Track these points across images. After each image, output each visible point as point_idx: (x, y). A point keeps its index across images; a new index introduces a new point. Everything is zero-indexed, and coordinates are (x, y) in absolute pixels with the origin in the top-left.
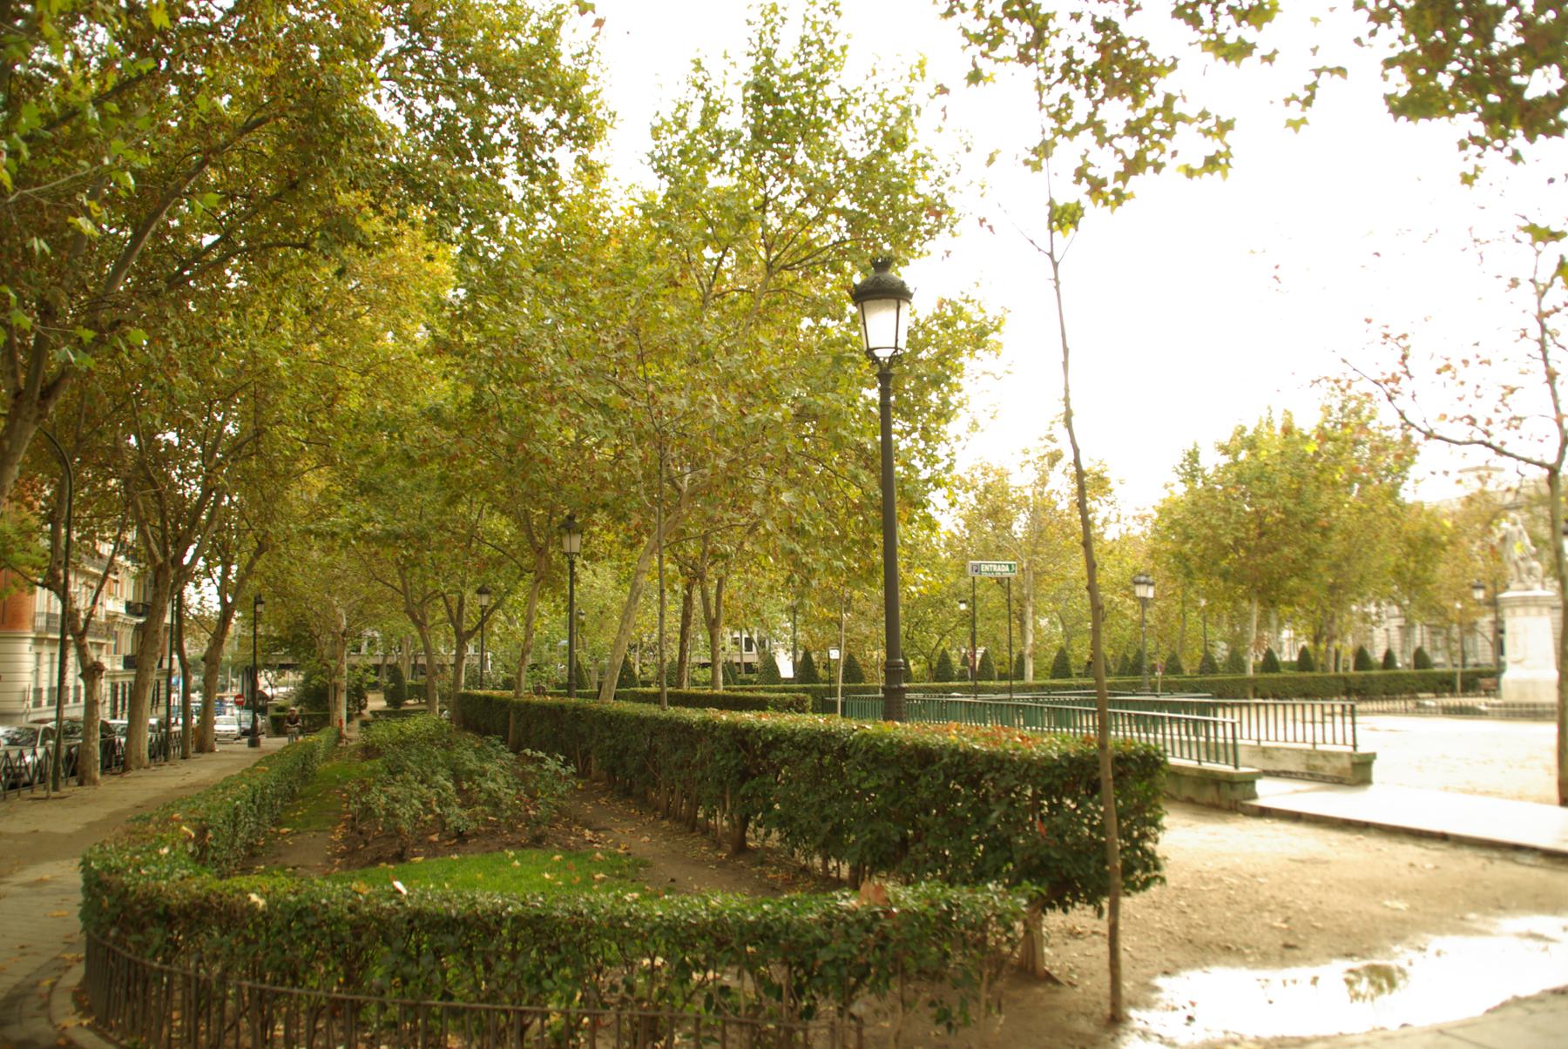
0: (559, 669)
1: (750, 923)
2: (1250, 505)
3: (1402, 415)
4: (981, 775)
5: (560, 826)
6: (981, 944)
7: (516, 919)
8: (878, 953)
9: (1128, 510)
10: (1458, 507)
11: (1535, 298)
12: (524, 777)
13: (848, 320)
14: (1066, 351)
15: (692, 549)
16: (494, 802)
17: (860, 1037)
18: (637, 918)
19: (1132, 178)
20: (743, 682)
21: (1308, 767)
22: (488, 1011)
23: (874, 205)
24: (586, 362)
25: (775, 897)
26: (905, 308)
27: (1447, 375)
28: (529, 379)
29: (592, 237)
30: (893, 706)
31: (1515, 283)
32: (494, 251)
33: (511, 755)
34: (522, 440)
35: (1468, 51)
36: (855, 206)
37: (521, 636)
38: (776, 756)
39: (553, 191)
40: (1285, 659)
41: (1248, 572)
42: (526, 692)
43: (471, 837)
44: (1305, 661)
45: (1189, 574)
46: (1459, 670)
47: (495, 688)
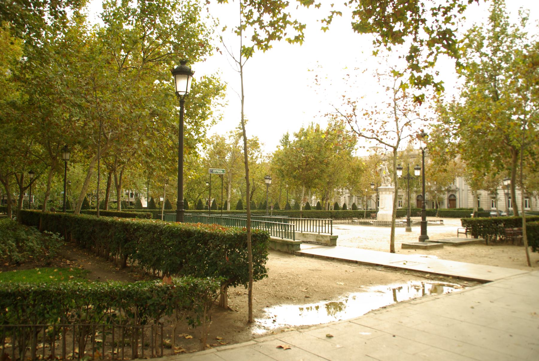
0: (60, 202)
1: (123, 291)
2: (304, 154)
3: (352, 128)
4: (208, 240)
5: (57, 259)
6: (205, 298)
7: (35, 292)
8: (168, 301)
9: (264, 154)
10: (368, 159)
11: (394, 94)
12: (44, 241)
13: (171, 81)
14: (243, 97)
15: (111, 160)
16: (32, 251)
17: (162, 330)
18: (82, 290)
19: (271, 41)
20: (129, 208)
21: (317, 240)
22: (23, 327)
23: (183, 41)
24: (74, 89)
25: (133, 282)
26: (191, 79)
27: (366, 116)
28: (52, 94)
29: (79, 43)
30: (179, 217)
31: (388, 89)
32: (39, 44)
33: (40, 233)
34: (47, 117)
35: (379, 13)
36: (176, 41)
37: (45, 190)
38: (138, 234)
39: (64, 23)
40: (313, 206)
41: (302, 176)
42: (47, 210)
43: (22, 263)
44: (319, 206)
45: (283, 176)
46: (365, 210)
47: (35, 209)
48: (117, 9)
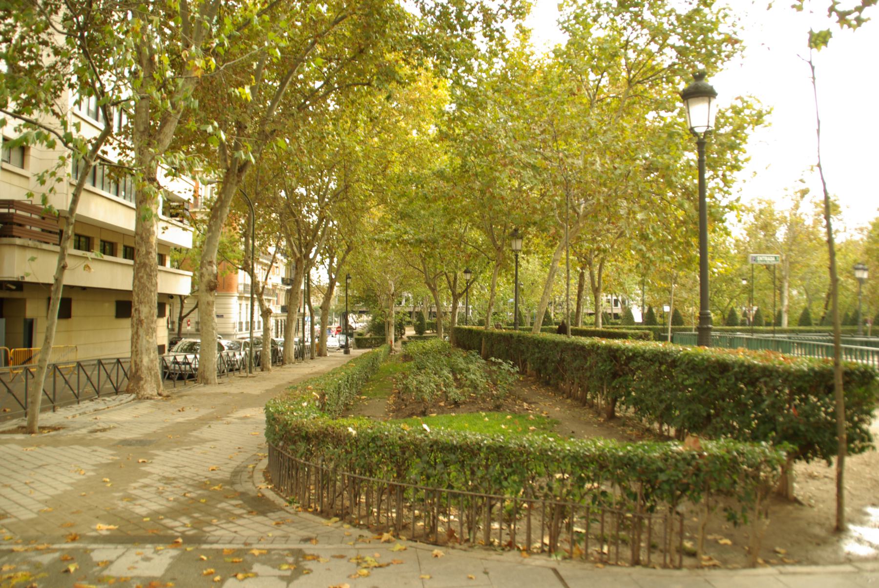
0: (509, 315)
1: (620, 456)
5: (510, 400)
7: (488, 447)
8: (694, 478)
12: (490, 373)
18: (556, 450)
20: (612, 324)
22: (472, 496)
24: (524, 142)
28: (491, 152)
29: (525, 71)
30: (703, 336)
33: (483, 361)
34: (489, 187)
37: (488, 296)
38: (633, 365)
42: (491, 327)
48: (579, 8)
